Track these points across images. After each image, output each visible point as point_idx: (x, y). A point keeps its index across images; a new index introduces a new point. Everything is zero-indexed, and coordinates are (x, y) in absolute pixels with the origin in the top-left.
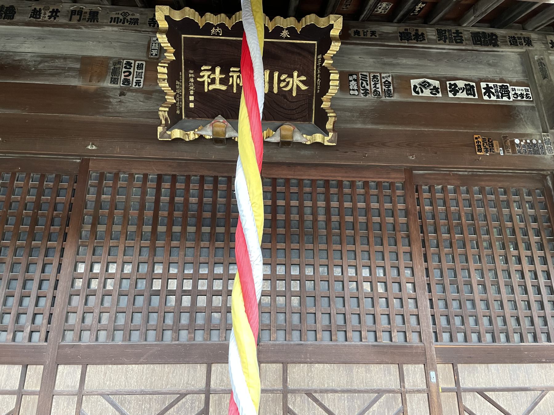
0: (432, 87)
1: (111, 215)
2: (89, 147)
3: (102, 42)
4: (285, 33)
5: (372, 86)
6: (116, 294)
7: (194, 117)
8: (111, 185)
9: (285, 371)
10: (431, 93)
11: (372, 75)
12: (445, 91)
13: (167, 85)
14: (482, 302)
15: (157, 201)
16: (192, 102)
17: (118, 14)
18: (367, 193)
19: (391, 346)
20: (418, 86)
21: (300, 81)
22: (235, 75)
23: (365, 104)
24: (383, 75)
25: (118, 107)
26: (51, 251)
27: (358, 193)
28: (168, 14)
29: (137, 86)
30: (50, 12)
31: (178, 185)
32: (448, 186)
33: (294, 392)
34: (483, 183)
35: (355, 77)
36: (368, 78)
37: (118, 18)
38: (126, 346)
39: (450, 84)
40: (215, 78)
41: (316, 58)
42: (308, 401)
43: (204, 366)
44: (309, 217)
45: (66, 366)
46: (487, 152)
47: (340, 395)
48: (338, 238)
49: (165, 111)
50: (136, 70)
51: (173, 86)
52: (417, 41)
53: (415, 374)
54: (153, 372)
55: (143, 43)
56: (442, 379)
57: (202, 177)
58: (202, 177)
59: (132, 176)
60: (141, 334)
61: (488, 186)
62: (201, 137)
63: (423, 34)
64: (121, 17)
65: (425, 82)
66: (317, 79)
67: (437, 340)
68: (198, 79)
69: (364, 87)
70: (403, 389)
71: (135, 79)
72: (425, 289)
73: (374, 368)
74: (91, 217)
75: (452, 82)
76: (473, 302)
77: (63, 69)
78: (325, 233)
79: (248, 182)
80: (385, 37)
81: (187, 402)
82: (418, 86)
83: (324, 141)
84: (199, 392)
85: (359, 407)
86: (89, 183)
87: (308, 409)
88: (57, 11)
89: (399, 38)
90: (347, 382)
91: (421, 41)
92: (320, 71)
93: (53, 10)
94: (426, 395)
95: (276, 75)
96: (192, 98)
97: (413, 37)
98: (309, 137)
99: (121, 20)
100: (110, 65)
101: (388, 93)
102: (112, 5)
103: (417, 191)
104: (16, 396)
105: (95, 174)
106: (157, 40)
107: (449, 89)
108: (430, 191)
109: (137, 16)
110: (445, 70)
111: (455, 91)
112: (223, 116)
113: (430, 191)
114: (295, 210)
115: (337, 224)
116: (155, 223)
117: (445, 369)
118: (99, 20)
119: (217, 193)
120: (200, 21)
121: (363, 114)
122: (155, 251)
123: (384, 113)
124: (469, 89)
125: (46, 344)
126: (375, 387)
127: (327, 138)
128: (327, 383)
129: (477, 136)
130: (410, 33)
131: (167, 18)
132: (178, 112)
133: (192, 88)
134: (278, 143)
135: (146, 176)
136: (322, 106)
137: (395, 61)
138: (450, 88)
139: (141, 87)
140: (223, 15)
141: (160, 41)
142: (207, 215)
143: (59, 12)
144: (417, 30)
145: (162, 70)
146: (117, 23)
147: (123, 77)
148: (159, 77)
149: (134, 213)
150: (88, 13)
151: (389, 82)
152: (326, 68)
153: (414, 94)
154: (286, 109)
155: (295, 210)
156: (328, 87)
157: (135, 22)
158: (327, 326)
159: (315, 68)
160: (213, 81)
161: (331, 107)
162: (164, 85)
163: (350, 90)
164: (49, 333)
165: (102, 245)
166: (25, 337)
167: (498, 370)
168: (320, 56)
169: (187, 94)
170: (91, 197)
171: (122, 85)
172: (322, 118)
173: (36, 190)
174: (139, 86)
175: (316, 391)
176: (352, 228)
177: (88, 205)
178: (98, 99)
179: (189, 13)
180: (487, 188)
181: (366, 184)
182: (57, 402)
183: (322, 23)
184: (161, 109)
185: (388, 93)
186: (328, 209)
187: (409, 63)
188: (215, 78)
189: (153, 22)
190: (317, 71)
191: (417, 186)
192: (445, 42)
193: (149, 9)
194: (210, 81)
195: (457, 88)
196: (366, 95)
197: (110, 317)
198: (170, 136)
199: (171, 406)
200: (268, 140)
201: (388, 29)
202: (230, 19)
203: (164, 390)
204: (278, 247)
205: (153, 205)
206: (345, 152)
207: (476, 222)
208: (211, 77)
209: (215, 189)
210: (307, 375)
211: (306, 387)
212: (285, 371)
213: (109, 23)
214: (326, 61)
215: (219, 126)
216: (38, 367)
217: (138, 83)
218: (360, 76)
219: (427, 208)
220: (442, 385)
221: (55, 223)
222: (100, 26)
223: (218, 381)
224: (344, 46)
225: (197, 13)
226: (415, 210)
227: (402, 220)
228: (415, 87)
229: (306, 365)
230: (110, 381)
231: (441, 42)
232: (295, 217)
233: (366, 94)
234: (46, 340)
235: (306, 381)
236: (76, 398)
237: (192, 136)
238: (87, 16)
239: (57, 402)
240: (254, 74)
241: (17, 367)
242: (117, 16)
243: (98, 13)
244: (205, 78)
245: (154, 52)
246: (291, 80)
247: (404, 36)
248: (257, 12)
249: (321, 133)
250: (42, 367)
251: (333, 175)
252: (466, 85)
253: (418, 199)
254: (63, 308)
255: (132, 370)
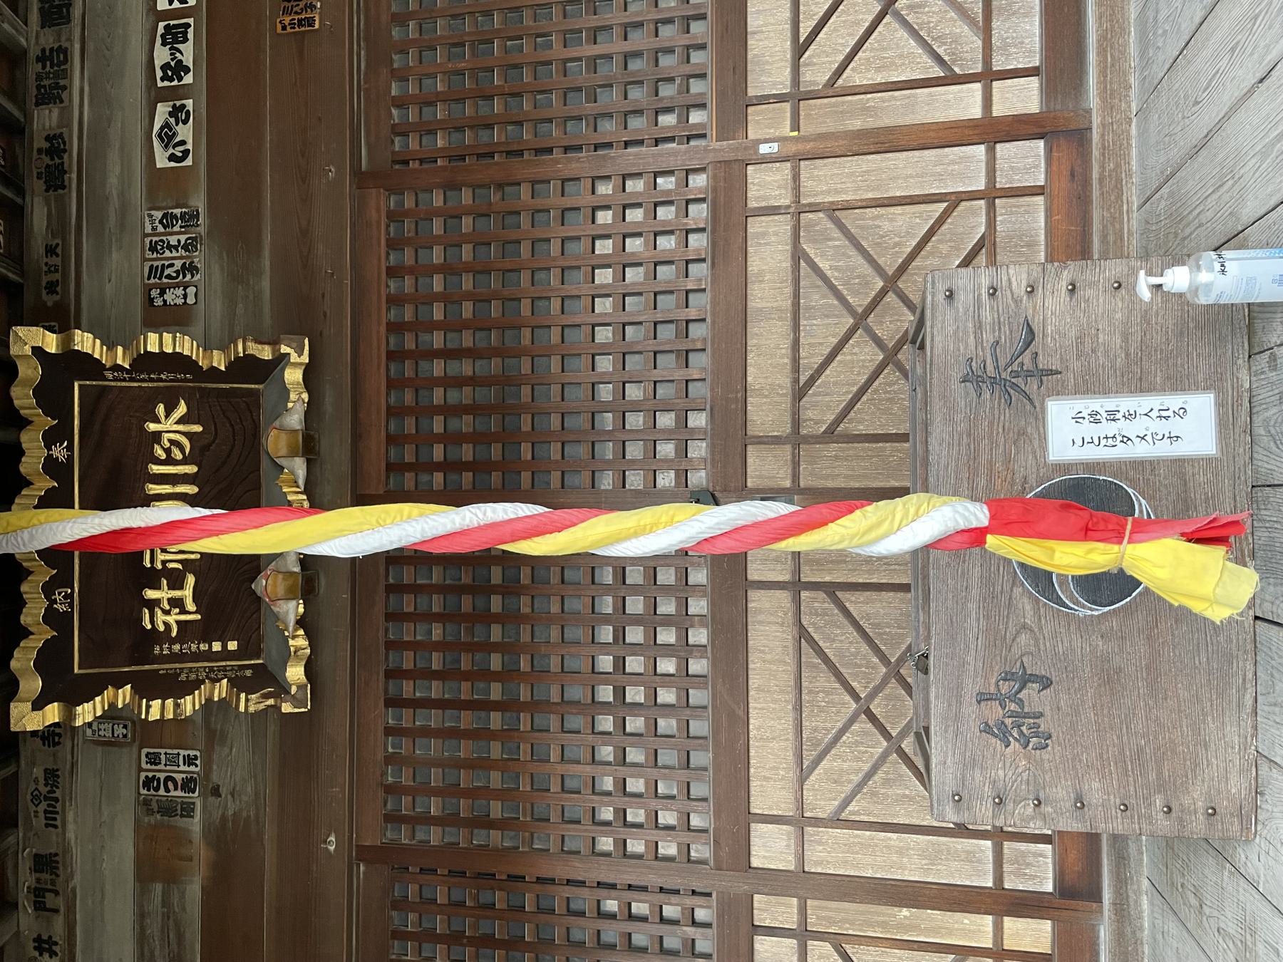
0: (172, 120)
1: (471, 793)
2: (332, 848)
3: (101, 843)
4: (59, 452)
5: (175, 254)
6: (622, 771)
7: (260, 640)
8: (410, 798)
9: (761, 441)
10: (185, 122)
11: (149, 255)
12: (181, 91)
13: (189, 698)
14: (629, 36)
15: (441, 704)
16: (224, 646)
17: (36, 812)
18: (411, 271)
19: (714, 231)
20: (171, 151)
21: (167, 417)
22: (161, 557)
23: (216, 269)
24: (148, 230)
25: (245, 798)
26: (544, 904)
27: (413, 290)
28: (29, 704)
29: (198, 762)
30: (41, 955)
31: (407, 664)
32: (393, 93)
33: (796, 423)
34: (385, 18)
35: (154, 293)
36: (155, 264)
37: (46, 812)
38: (716, 745)
39: (162, 80)
40: (169, 600)
41: (113, 384)
42: (814, 395)
43: (753, 595)
44: (465, 395)
45: (753, 853)
46: (312, 7)
47: (802, 334)
48: (508, 333)
49: (247, 700)
50: (161, 767)
51: (191, 687)
52: (65, 151)
53: (766, 185)
54: (763, 691)
55: (99, 755)
56: (776, 129)
57: (390, 617)
58: (390, 617)
59: (389, 759)
60: (696, 717)
61: (389, 7)
62: (300, 623)
63: (48, 138)
64: (43, 806)
65: (160, 136)
66: (161, 380)
67: (704, 136)
68: (174, 634)
69: (177, 272)
70: (791, 210)
71: (182, 768)
72: (604, 156)
73: (754, 265)
74: (476, 831)
75: (159, 74)
76: (627, 56)
77: (166, 917)
78: (499, 360)
79: (340, 533)
80: (59, 224)
81: (814, 624)
82: (171, 151)
83: (301, 364)
84: (797, 602)
85: (824, 297)
86: (407, 842)
87: (827, 394)
88: (38, 939)
89: (60, 191)
90: (780, 319)
91: (64, 143)
92: (142, 373)
93: (35, 948)
94: (802, 163)
95: (156, 469)
96: (217, 646)
97: (57, 161)
98: (293, 396)
99: (49, 805)
100: (153, 822)
101: (190, 219)
102: (17, 826)
103: (406, 162)
104: (810, 943)
105: (389, 834)
106: (90, 725)
107: (175, 83)
108: (405, 134)
109: (38, 772)
110: (133, 88)
111: (177, 69)
112: (253, 579)
113: (405, 134)
114: (454, 424)
115: (479, 335)
116: (487, 706)
117: (757, 122)
118: (53, 851)
119: (420, 585)
120: (41, 635)
121: (239, 276)
122: (539, 703)
123: (236, 228)
124: (174, 37)
125: (714, 895)
126: (787, 264)
127: (294, 358)
128: (782, 357)
129: (279, 26)
130: (48, 166)
131: (38, 705)
132: (248, 673)
133: (194, 647)
134: (309, 461)
135: (389, 731)
136: (223, 368)
137: (115, 202)
138: (171, 80)
139: (198, 754)
140: (24, 588)
141: (89, 718)
142: (466, 603)
143: (39, 936)
144: (40, 151)
145: (155, 710)
146: (57, 813)
147: (179, 793)
148: (171, 716)
149: (465, 749)
150: (38, 875)
151: (165, 216)
152: (134, 360)
153: (189, 162)
154: (233, 446)
155: (454, 424)
156: (177, 356)
157: (52, 776)
158: (677, 357)
159: (136, 384)
160: (177, 603)
161: (223, 348)
162: (189, 704)
163: (185, 303)
164: (698, 890)
165: (528, 806)
166: (703, 934)
167: (758, 12)
168: (109, 375)
169: (210, 656)
170: (434, 836)
171: (196, 794)
172: (247, 368)
173: (424, 945)
174: (196, 758)
175: (796, 381)
176: (486, 304)
177: (452, 840)
178: (229, 843)
179: (23, 660)
180: (393, 9)
181: (392, 272)
182: (817, 863)
183: (30, 371)
184: (242, 709)
185: (190, 219)
186: (448, 354)
187: (117, 169)
188: (169, 600)
189: (50, 735)
190: (143, 380)
191: (395, 162)
192: (64, 88)
193: (21, 745)
194: (177, 610)
195: (173, 64)
196: (197, 270)
197: (665, 778)
198: (301, 687)
199: (820, 652)
200: (301, 482)
201: (39, 216)
202: (32, 572)
203: (792, 668)
204: (529, 457)
205: (448, 712)
206: (325, 316)
207: (466, 38)
208: (168, 607)
209: (415, 589)
210: (766, 397)
211: (789, 399)
212: (761, 441)
213: (60, 830)
214: (119, 362)
215: (275, 585)
216: (756, 905)
217: (190, 761)
218: (152, 281)
219: (440, 143)
220: (786, 131)
221: (490, 901)
222: (67, 850)
223: (779, 567)
224: (84, 321)
225: (22, 644)
226: (443, 168)
227: (466, 197)
228: (172, 158)
229: (749, 399)
230: (778, 769)
231: (65, 95)
232: (466, 424)
233: (190, 268)
234: (709, 895)
235: (777, 399)
236: (808, 829)
237: (300, 642)
238: (46, 876)
239: (817, 863)
240: (134, 526)
241: (757, 946)
242: (41, 815)
243: (36, 855)
244: (171, 619)
245: (120, 731)
246: (166, 436)
247: (55, 179)
248: (8, 523)
249: (283, 370)
250: (756, 897)
251: (375, 344)
252: (164, 44)
253: (422, 161)
254: (648, 867)
255: (758, 729)
